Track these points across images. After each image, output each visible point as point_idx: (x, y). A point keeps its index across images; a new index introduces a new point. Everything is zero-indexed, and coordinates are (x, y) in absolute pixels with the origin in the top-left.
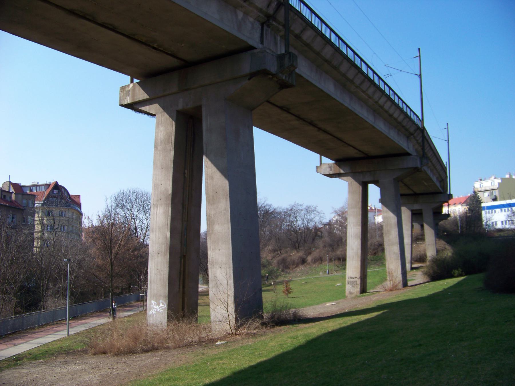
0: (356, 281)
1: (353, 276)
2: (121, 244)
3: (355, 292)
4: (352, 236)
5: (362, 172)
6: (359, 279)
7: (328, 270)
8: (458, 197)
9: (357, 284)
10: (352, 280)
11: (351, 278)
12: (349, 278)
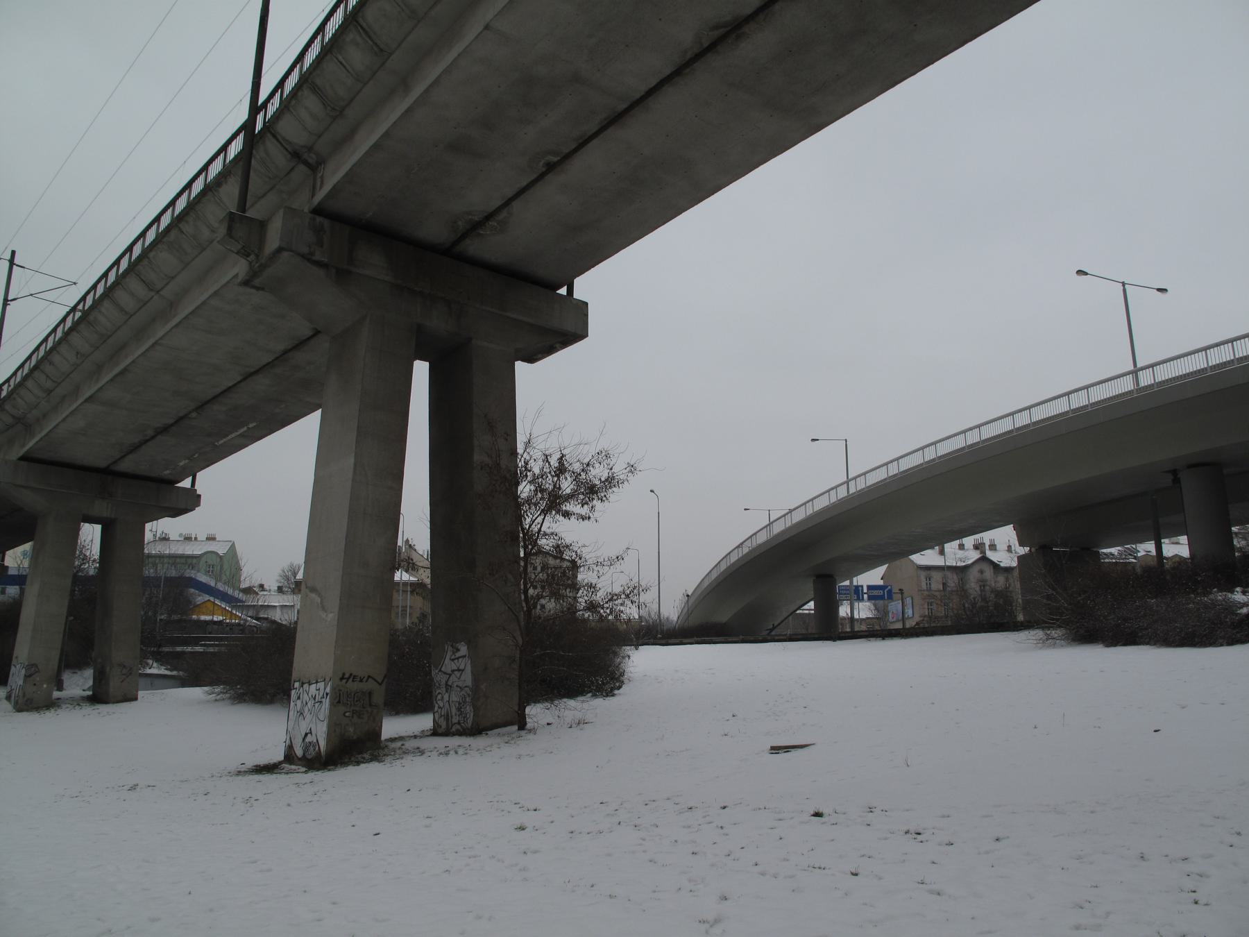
6: (380, 684)
10: (353, 686)
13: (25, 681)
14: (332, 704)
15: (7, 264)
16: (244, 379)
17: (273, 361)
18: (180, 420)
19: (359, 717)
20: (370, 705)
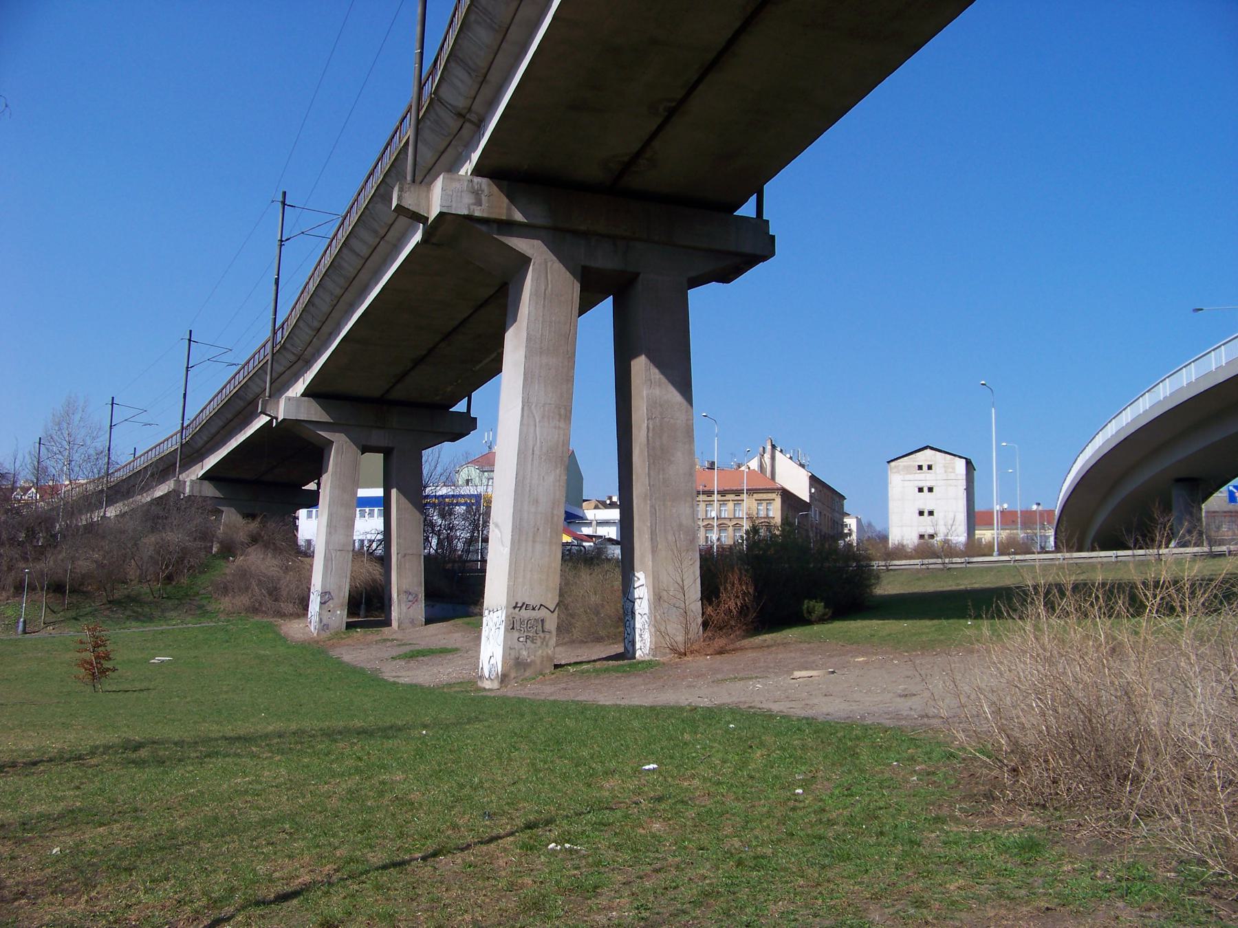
1: (532, 602)
3: (538, 662)
4: (537, 452)
5: (585, 235)
6: (552, 612)
7: (22, 620)
10: (525, 614)
12: (515, 608)
13: (320, 608)
14: (506, 630)
15: (280, 205)
16: (475, 312)
17: (494, 294)
18: (430, 351)
19: (532, 642)
20: (543, 631)
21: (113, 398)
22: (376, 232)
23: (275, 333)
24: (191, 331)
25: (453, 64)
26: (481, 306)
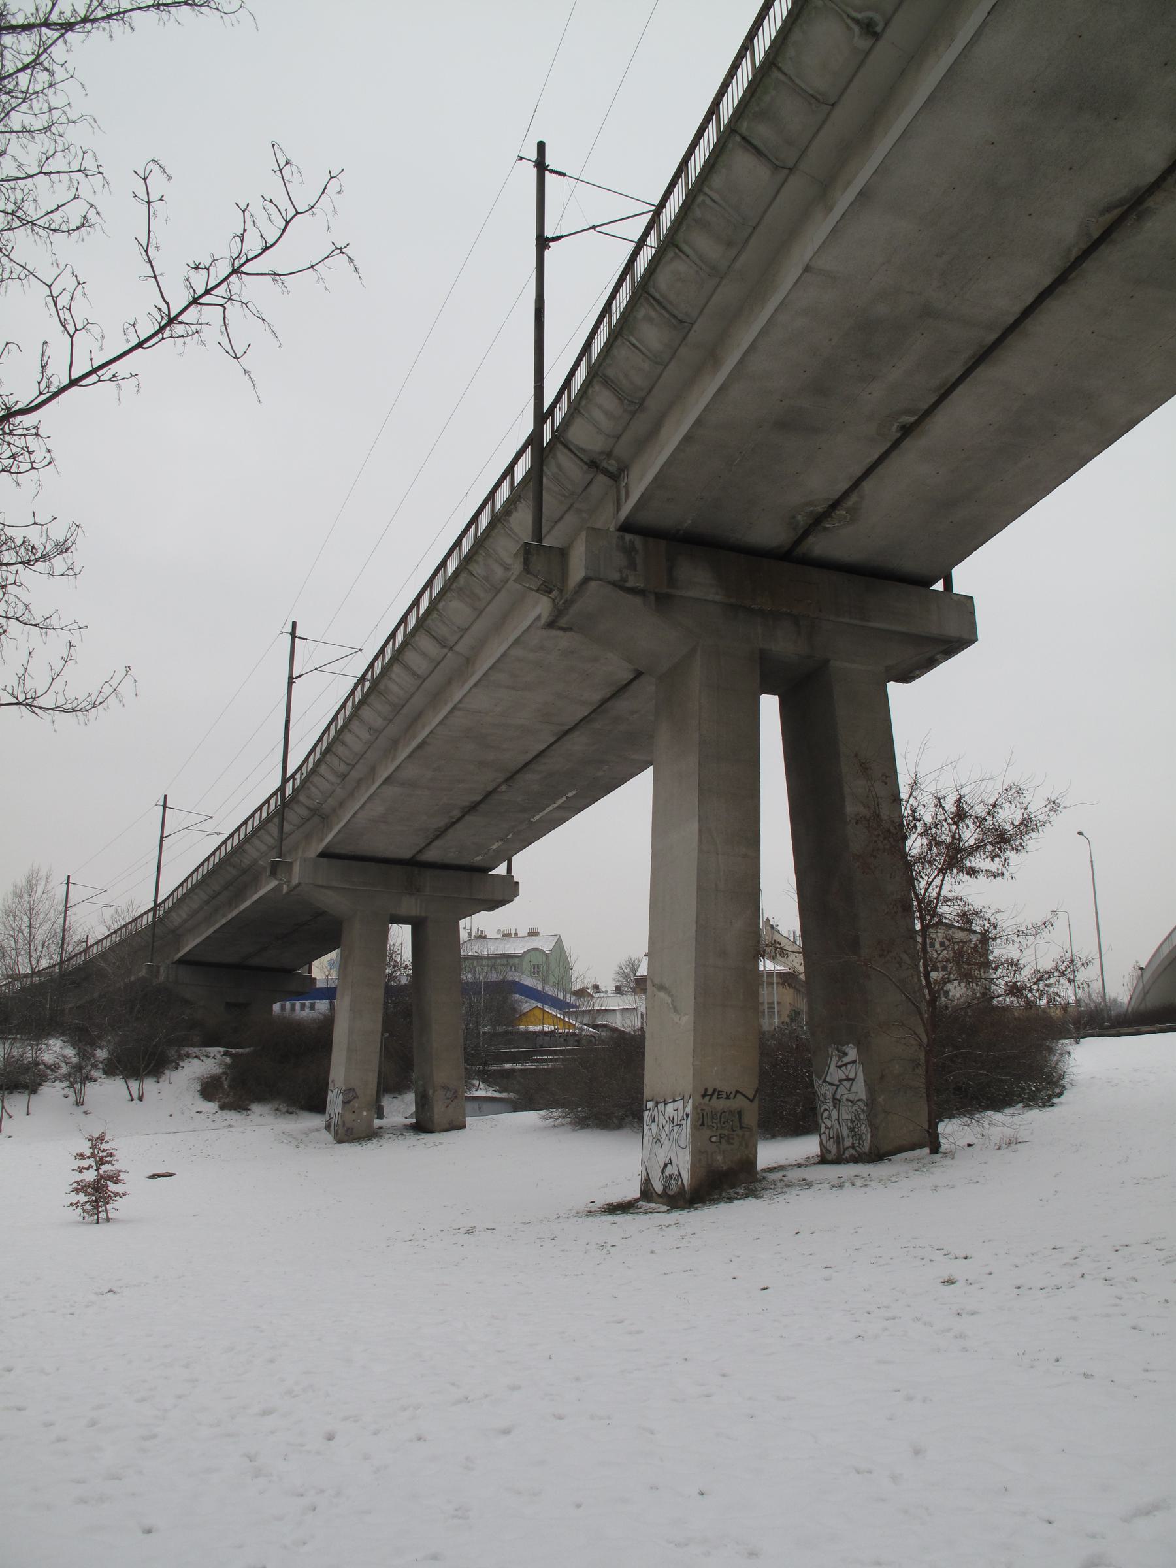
0: (740, 1113)
1: (725, 1087)
2: (49, 1070)
6: (751, 1101)
8: (645, 955)
9: (741, 1128)
10: (720, 1104)
11: (718, 1093)
13: (343, 1108)
19: (729, 1143)
21: (69, 877)
22: (407, 668)
23: (285, 781)
24: (166, 796)
25: (597, 387)
26: (566, 733)
